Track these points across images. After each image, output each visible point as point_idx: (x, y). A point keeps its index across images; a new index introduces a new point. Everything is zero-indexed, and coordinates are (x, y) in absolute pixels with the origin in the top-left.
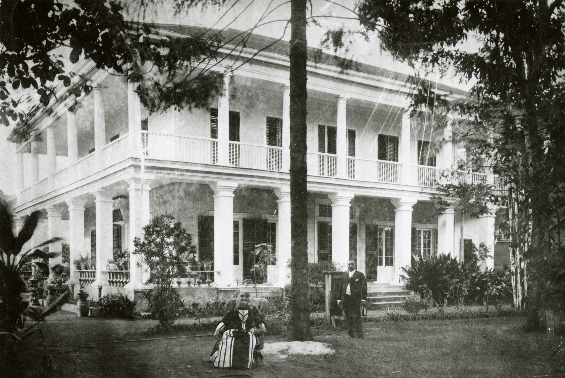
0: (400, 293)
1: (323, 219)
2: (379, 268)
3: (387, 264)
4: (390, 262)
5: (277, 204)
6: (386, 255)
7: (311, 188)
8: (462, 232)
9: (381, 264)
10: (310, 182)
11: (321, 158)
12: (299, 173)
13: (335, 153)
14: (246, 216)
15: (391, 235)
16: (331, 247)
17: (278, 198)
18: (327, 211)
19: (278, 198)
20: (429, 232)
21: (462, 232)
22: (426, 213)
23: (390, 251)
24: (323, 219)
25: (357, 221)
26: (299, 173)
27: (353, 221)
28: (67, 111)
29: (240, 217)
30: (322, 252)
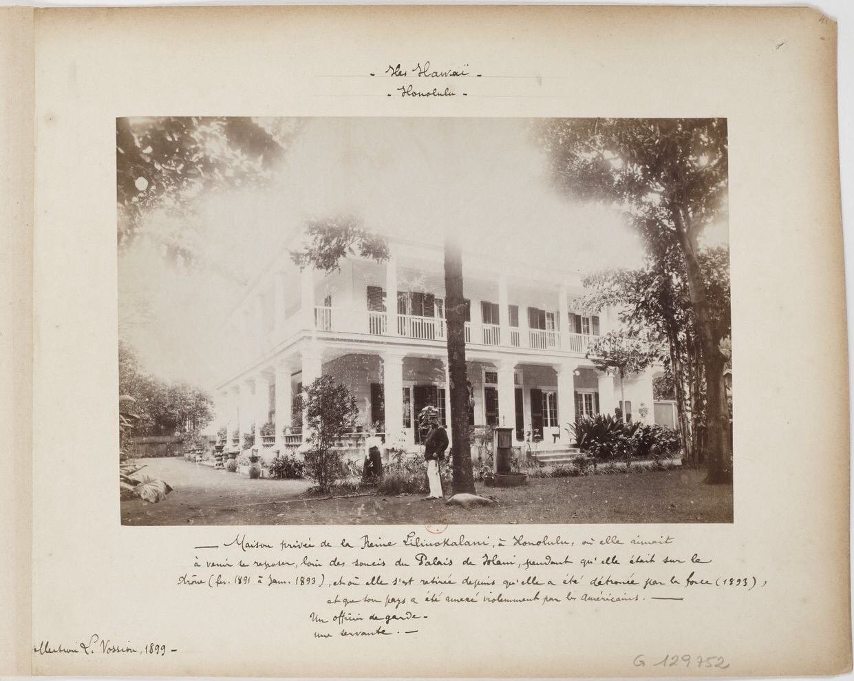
0: (567, 451)
1: (490, 385)
2: (544, 428)
3: (552, 425)
4: (554, 423)
5: (557, 377)
6: (551, 417)
7: (469, 356)
8: (622, 393)
9: (546, 425)
10: (468, 349)
11: (401, 322)
12: (456, 345)
13: (498, 324)
14: (416, 383)
15: (554, 398)
16: (498, 410)
17: (557, 373)
18: (492, 377)
19: (557, 373)
20: (590, 395)
21: (622, 393)
22: (586, 377)
23: (554, 414)
24: (490, 385)
25: (521, 386)
26: (456, 345)
27: (518, 386)
28: (417, 319)
29: (411, 385)
30: (536, 415)
